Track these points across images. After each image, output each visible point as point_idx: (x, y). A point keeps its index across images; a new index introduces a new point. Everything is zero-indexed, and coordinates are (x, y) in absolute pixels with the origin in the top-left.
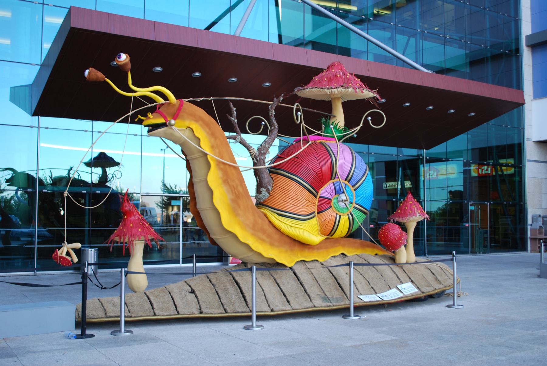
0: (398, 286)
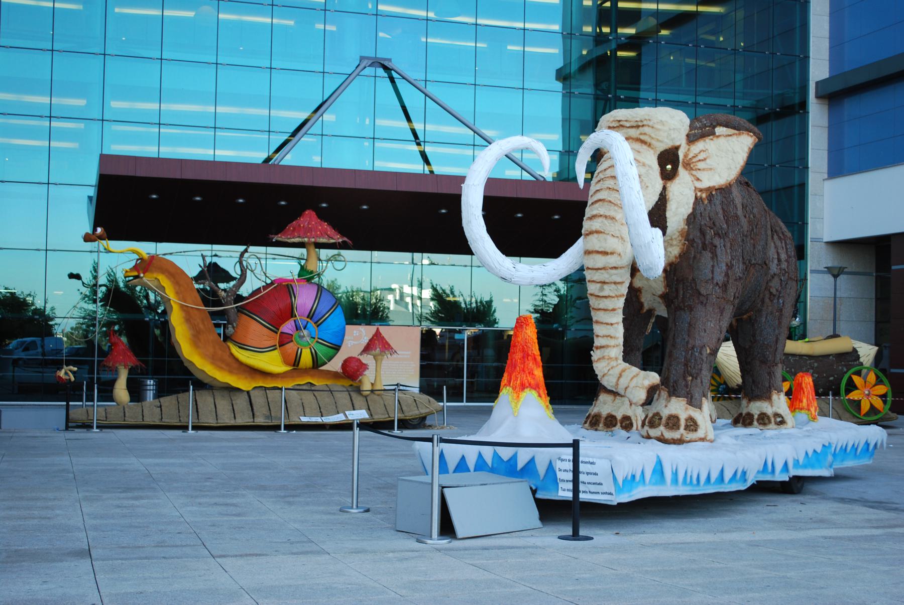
0: (347, 413)
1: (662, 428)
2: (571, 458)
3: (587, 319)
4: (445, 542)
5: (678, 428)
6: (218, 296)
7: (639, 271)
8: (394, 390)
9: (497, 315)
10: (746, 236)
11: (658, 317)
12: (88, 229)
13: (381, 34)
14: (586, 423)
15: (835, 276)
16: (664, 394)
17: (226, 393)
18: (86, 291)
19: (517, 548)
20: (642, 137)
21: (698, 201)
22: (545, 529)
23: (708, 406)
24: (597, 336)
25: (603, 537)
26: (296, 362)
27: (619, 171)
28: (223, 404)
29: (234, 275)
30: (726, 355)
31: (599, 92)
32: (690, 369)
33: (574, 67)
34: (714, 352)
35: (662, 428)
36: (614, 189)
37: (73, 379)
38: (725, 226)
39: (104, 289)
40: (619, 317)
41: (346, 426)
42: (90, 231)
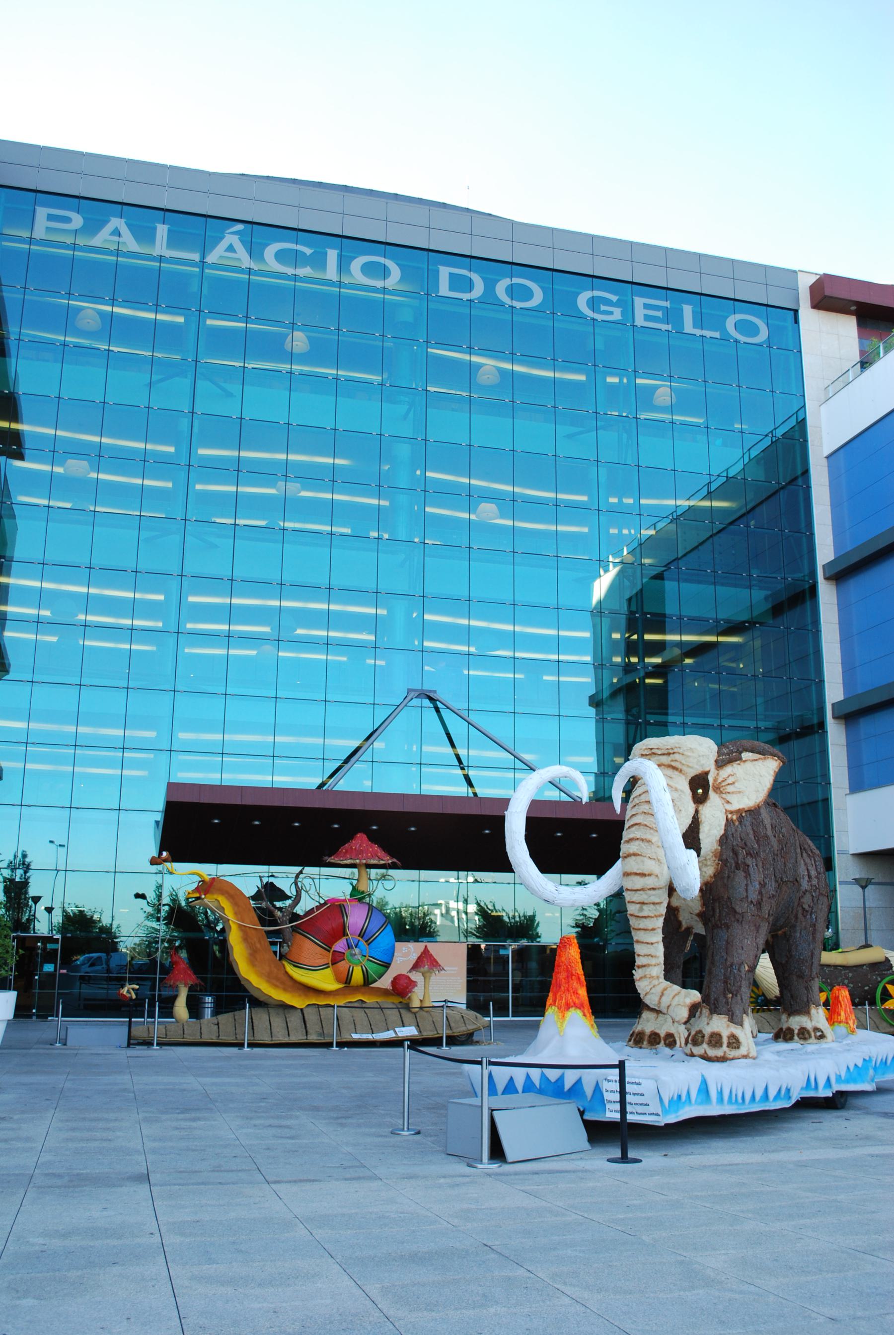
1: (705, 1046)
2: (618, 1078)
3: (626, 931)
4: (495, 1167)
5: (721, 1046)
6: (273, 916)
7: (675, 890)
8: (442, 1007)
9: (540, 930)
10: (777, 855)
11: (696, 935)
12: (155, 854)
13: (426, 668)
14: (630, 1040)
15: (864, 888)
16: (706, 1011)
17: (281, 1011)
18: (150, 910)
19: (566, 1171)
20: (673, 764)
21: (729, 822)
22: (594, 1151)
23: (749, 1022)
24: (639, 955)
25: (651, 1159)
26: (348, 980)
27: (653, 797)
28: (278, 1022)
29: (289, 894)
30: (763, 967)
31: (630, 717)
32: (730, 987)
33: (606, 694)
34: (753, 969)
35: (705, 1046)
36: (649, 814)
37: (134, 997)
38: (756, 846)
39: (167, 908)
40: (658, 937)
41: (397, 1043)
42: (156, 855)
